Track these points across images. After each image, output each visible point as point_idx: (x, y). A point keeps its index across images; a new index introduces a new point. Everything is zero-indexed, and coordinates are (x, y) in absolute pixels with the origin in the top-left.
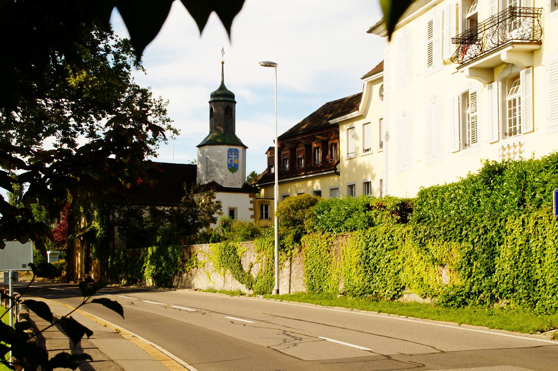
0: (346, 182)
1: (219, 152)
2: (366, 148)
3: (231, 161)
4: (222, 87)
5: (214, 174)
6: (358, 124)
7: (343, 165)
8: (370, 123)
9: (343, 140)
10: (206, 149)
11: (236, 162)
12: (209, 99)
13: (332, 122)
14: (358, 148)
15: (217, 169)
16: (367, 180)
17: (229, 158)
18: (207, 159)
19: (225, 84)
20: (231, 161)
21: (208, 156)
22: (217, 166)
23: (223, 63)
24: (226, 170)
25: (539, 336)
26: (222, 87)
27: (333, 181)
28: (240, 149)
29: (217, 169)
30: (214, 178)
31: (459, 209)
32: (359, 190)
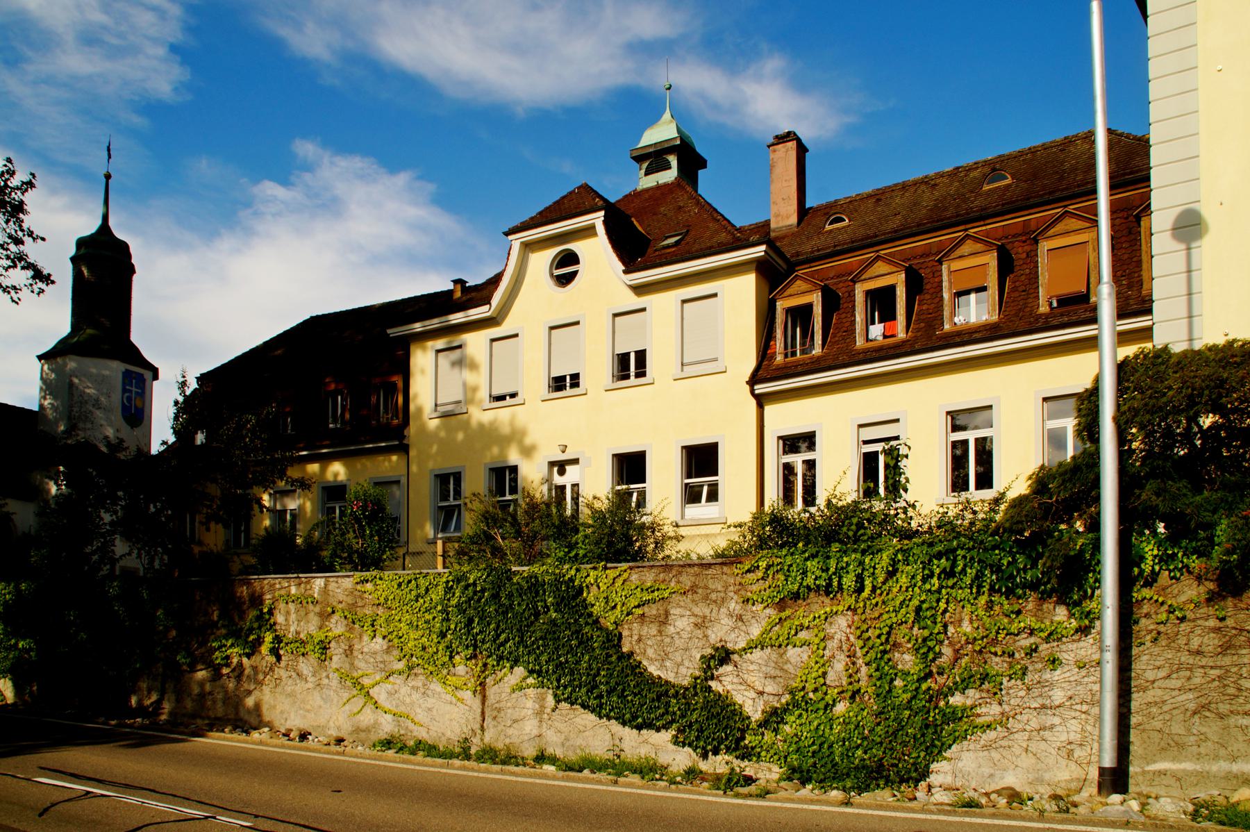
0: (431, 465)
1: (107, 373)
2: (496, 392)
3: (129, 399)
4: (105, 228)
5: (89, 425)
6: (475, 342)
7: (422, 428)
8: (577, 323)
9: (423, 372)
10: (72, 364)
11: (139, 404)
12: (72, 251)
13: (393, 332)
14: (475, 389)
15: (99, 413)
16: (505, 461)
17: (124, 390)
18: (71, 385)
19: (112, 223)
20: (129, 399)
21: (76, 381)
22: (97, 404)
23: (108, 177)
24: (117, 416)
25: (229, 736)
26: (105, 228)
27: (390, 464)
28: (148, 375)
29: (99, 413)
30: (89, 433)
31: (1206, 510)
32: (476, 483)
